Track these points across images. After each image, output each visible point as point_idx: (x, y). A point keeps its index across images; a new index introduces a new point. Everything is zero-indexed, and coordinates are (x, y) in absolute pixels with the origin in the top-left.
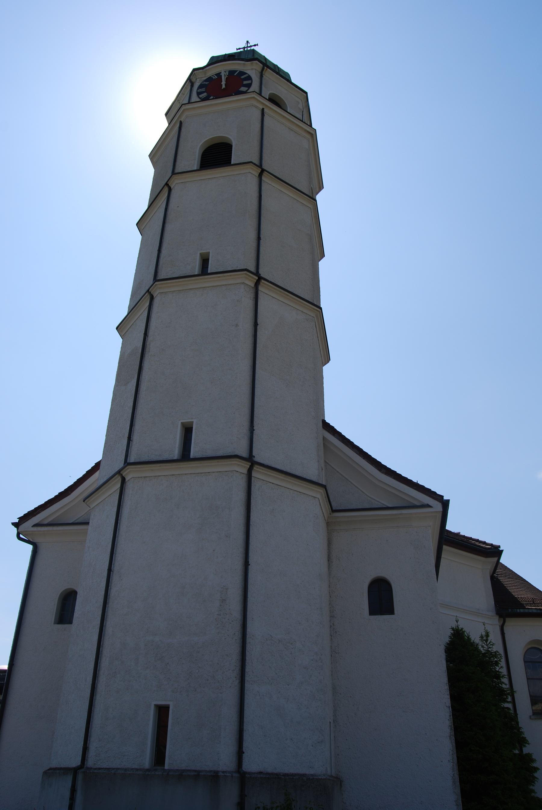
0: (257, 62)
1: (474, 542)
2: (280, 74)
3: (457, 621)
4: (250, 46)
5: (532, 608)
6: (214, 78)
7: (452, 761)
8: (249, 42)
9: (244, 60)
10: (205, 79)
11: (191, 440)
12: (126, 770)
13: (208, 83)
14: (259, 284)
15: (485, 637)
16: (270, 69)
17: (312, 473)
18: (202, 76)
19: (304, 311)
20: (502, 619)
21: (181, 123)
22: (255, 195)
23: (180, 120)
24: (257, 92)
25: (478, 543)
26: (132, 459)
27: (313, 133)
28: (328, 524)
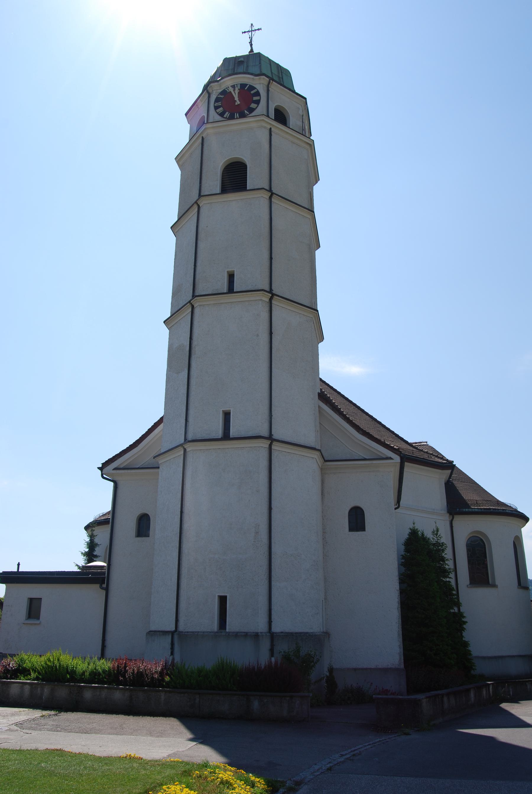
0: (264, 77)
1: (434, 457)
2: (285, 86)
3: (414, 524)
4: (254, 30)
5: (474, 508)
6: (228, 91)
7: (398, 623)
8: (253, 24)
9: (253, 75)
10: (220, 91)
11: (230, 422)
12: (203, 632)
13: (223, 96)
14: (272, 299)
15: (436, 532)
16: (275, 82)
17: (311, 439)
18: (218, 88)
19: (305, 314)
20: (451, 516)
21: (203, 138)
22: (267, 217)
23: (202, 136)
24: (266, 115)
25: (437, 458)
26: (190, 437)
27: (311, 143)
28: (322, 469)
